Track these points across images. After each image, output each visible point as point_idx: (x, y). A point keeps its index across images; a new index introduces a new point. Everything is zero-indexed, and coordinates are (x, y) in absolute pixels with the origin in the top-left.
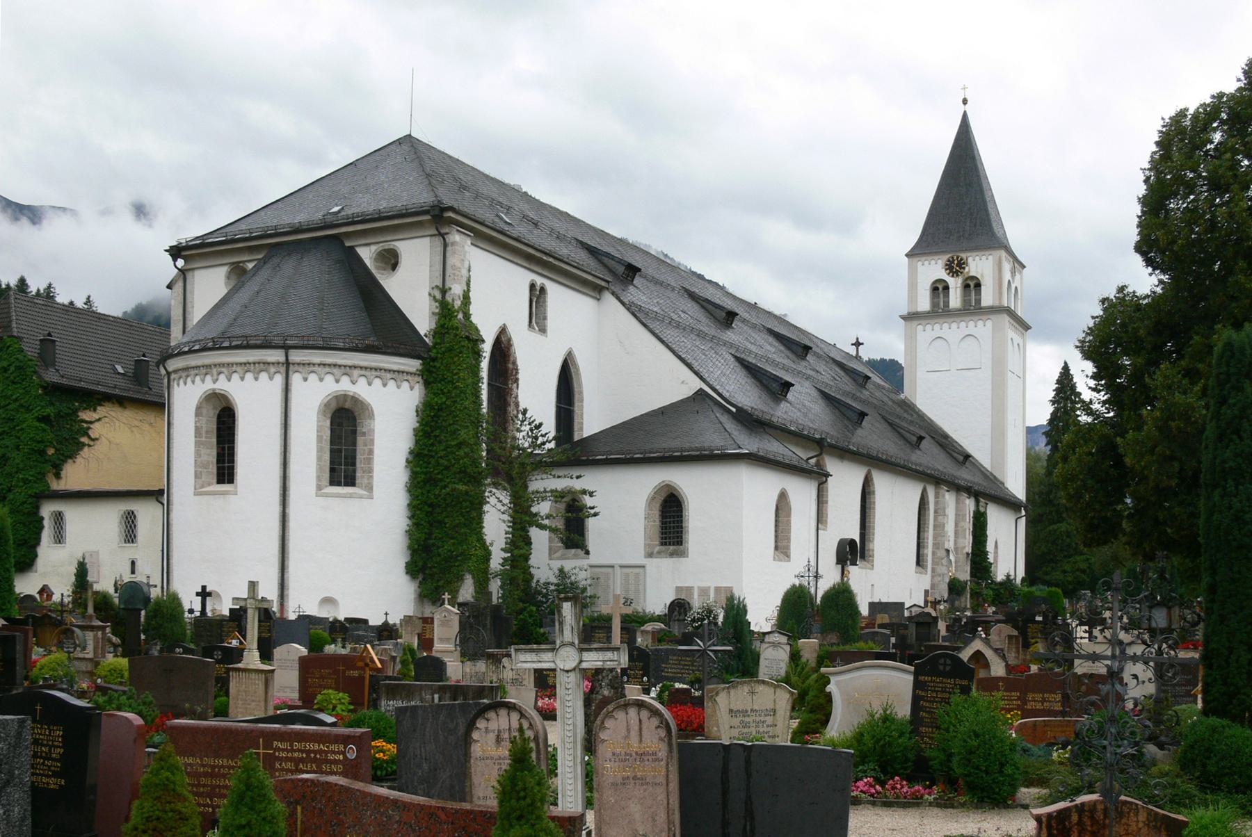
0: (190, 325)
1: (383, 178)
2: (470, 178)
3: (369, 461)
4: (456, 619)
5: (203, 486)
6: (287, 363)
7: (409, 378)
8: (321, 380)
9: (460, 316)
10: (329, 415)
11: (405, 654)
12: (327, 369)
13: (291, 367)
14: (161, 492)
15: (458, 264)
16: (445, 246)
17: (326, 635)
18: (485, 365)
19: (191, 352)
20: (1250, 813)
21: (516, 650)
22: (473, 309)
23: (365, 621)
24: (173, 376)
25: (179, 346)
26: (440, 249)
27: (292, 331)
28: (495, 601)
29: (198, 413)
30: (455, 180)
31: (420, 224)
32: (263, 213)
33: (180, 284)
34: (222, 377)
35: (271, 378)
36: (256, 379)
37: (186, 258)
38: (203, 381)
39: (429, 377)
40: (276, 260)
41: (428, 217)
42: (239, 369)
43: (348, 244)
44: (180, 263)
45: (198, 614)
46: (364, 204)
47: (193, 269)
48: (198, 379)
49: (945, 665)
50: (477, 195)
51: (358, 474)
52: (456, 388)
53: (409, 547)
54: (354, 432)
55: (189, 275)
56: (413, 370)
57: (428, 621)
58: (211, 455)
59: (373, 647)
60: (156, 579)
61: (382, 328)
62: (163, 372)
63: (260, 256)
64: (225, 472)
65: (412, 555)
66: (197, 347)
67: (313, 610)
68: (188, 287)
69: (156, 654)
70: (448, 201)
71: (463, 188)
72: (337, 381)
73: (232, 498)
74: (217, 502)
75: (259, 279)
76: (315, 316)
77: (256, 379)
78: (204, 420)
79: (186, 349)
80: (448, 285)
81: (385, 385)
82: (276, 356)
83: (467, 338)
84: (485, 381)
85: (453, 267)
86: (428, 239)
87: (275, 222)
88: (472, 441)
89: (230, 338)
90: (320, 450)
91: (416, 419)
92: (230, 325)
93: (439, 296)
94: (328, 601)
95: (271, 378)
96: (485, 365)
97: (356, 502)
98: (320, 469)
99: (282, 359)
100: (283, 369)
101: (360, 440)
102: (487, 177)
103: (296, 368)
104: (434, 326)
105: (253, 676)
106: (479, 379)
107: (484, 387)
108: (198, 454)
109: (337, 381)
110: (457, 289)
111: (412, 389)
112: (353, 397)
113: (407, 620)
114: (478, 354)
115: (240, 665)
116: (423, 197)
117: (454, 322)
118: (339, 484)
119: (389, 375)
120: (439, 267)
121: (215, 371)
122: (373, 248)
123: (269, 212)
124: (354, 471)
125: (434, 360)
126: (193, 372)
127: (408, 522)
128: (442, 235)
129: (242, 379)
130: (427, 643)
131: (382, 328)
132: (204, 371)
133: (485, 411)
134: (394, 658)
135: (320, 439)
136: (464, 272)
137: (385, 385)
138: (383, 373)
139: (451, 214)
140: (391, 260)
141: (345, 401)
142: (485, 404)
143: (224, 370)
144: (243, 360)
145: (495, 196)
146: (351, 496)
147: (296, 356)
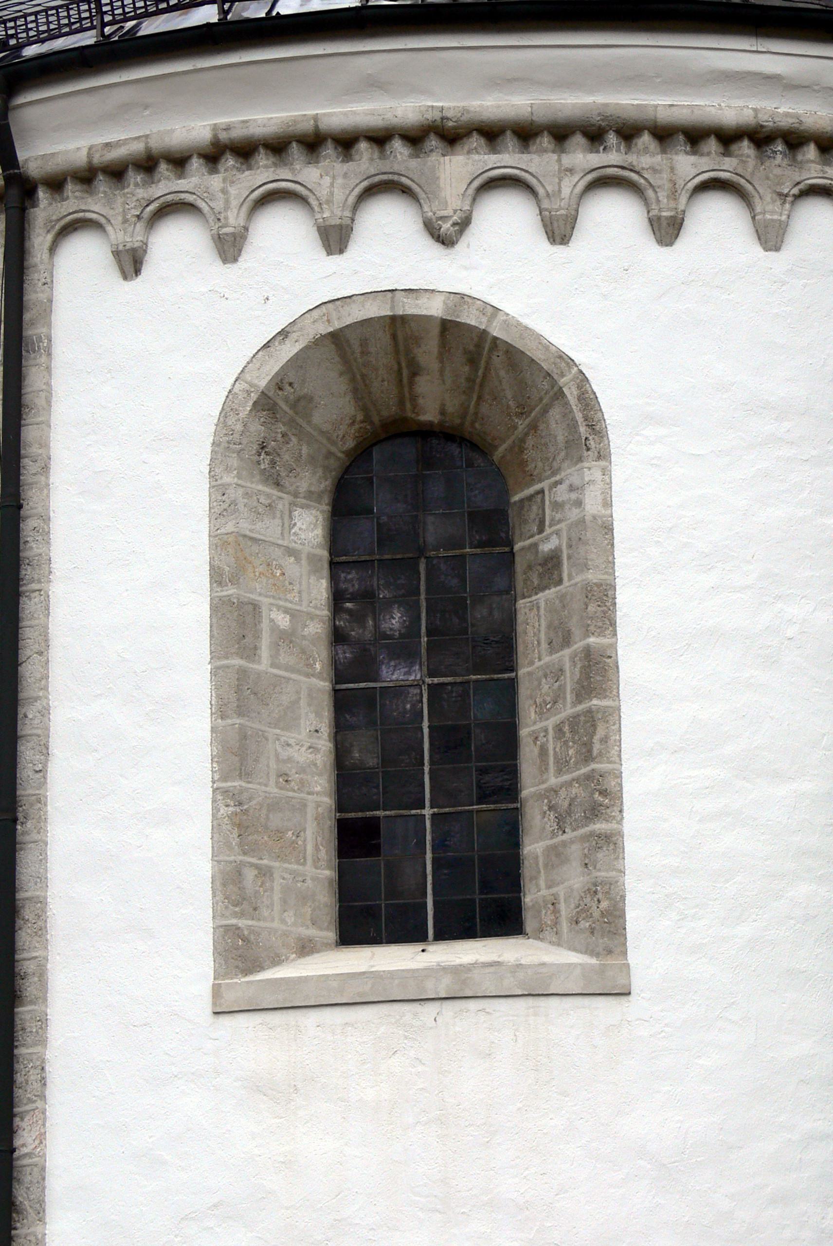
3: (590, 734)
10: (313, 480)
12: (265, 173)
20: (312, 3)
72: (335, 238)
90: (239, 698)
101: (534, 615)
103: (74, 201)
109: (335, 238)
112: (448, 328)
118: (407, 930)
124: (511, 832)
138: (646, 156)
141: (408, 370)
146: (459, 992)
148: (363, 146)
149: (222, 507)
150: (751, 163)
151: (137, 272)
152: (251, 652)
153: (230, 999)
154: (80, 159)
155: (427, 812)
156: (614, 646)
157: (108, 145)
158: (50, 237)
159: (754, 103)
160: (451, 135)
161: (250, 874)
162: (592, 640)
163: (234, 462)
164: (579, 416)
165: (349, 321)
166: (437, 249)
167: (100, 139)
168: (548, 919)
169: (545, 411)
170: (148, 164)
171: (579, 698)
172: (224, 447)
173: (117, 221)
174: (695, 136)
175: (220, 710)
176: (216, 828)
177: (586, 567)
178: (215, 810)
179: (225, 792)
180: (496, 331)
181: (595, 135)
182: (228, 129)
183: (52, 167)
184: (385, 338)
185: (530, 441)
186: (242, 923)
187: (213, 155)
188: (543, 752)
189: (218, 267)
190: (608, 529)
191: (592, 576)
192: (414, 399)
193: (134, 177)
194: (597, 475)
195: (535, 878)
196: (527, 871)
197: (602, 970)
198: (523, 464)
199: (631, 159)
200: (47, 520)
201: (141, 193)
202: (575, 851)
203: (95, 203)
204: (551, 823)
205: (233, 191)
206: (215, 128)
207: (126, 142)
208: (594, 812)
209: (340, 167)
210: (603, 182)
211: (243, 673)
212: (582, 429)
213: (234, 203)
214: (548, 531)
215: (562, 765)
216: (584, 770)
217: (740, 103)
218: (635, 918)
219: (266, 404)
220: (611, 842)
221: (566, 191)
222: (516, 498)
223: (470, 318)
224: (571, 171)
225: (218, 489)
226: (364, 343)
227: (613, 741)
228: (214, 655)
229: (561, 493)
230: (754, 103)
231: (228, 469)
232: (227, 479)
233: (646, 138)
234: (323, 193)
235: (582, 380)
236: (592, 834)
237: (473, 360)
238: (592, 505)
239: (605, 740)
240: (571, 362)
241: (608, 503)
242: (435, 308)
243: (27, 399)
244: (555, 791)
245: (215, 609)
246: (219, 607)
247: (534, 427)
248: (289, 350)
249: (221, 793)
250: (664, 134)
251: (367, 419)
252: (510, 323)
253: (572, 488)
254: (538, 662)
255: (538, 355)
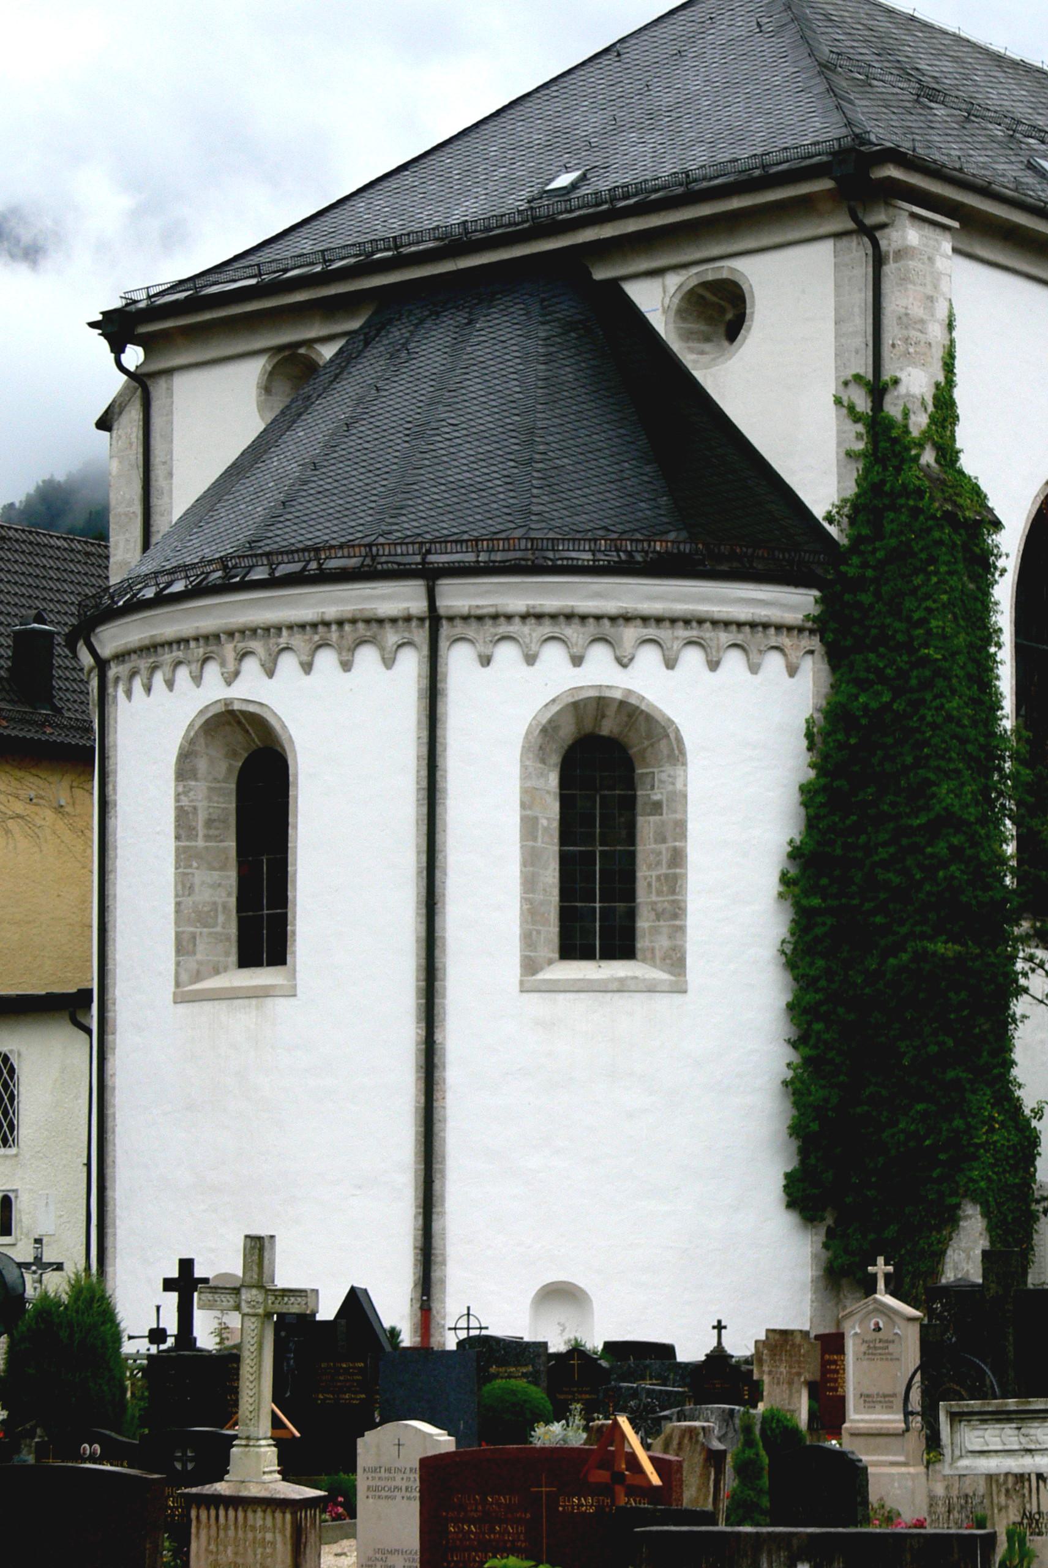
0: (162, 525)
1: (695, 85)
2: (947, 66)
3: (674, 883)
4: (911, 1337)
5: (198, 977)
6: (434, 619)
7: (785, 640)
8: (531, 659)
9: (928, 457)
10: (555, 759)
11: (749, 1443)
12: (547, 629)
13: (445, 630)
14: (85, 995)
15: (917, 311)
16: (879, 260)
17: (537, 1394)
18: (1004, 592)
19: (162, 600)
21: (956, 1417)
22: (965, 436)
23: (668, 1351)
24: (113, 671)
25: (128, 585)
26: (863, 271)
27: (447, 526)
28: (870, 1268)
29: (185, 768)
30: (905, 73)
31: (803, 207)
32: (360, 204)
33: (132, 416)
34: (251, 666)
35: (389, 662)
36: (346, 666)
37: (148, 343)
38: (197, 679)
39: (841, 637)
40: (397, 333)
41: (825, 184)
42: (298, 640)
43: (600, 274)
44: (134, 356)
45: (170, 1342)
46: (644, 159)
47: (169, 372)
48: (183, 675)
49: (184, 1461)
50: (971, 113)
51: (643, 924)
52: (925, 661)
53: (797, 1130)
54: (629, 805)
55: (158, 390)
56: (794, 618)
57: (832, 1344)
58: (220, 887)
59: (648, 1427)
60: (69, 1248)
61: (705, 506)
62: (86, 659)
63: (355, 325)
64: (262, 931)
65: (804, 1153)
66: (178, 587)
67: (510, 1318)
68: (157, 422)
69: (31, 1459)
70: (883, 132)
71: (929, 94)
72: (577, 661)
73: (281, 1005)
74: (239, 1020)
75: (350, 387)
76: (510, 481)
77: (346, 666)
78: (200, 789)
79: (149, 593)
80: (889, 371)
81: (714, 665)
82: (402, 598)
83: (950, 517)
84: (1007, 637)
85: (905, 320)
86: (828, 246)
87: (395, 227)
88: (972, 813)
89: (274, 557)
90: (530, 858)
91: (805, 757)
92: (273, 520)
93: (862, 403)
94: (560, 1295)
95: (389, 662)
96: (1004, 592)
97: (636, 1003)
98: (531, 913)
99: (418, 606)
100: (421, 635)
101: (646, 826)
102: (999, 60)
103: (459, 629)
104: (851, 490)
105: (257, 1518)
106: (988, 636)
107: (1005, 656)
108: (184, 886)
109: (577, 661)
110: (916, 382)
111: (792, 671)
112: (622, 704)
113: (779, 1342)
114: (983, 565)
115: (221, 1488)
116: (804, 125)
117: (911, 476)
118: (585, 953)
119: (724, 637)
120: (862, 323)
121: (229, 650)
122: (673, 281)
123: (378, 199)
124: (631, 915)
125: (858, 584)
126: (168, 657)
127: (788, 1054)
128: (870, 233)
129: (307, 667)
130: (829, 1410)
131: (705, 506)
132: (201, 652)
133: (1008, 724)
134: (715, 1459)
135: (529, 826)
136: (936, 332)
137: (714, 665)
139: (893, 172)
140: (723, 311)
142: (1008, 704)
143: (255, 645)
144: (307, 613)
145: (1021, 110)
146: (621, 987)
147: (457, 596)
148: (591, 620)
149: (525, 776)
150: (749, 636)
151: (488, 663)
152: (535, 839)
153: (527, 986)
154: (465, 611)
155: (598, 905)
156: (685, 847)
157: (477, 607)
158: (448, 643)
159: (752, 611)
160: (627, 618)
161: (534, 933)
162: (677, 844)
163: (531, 755)
164: (675, 747)
165: (581, 697)
166: (620, 668)
167: (474, 603)
168: (649, 955)
169: (659, 740)
170: (495, 617)
171: (669, 867)
172: (526, 750)
173: (481, 641)
174: (727, 624)
175: (524, 864)
176: (522, 914)
177: (675, 812)
178: (522, 906)
179: (526, 899)
180: (643, 707)
181: (687, 622)
182: (534, 607)
183: (451, 612)
184: (594, 705)
185: (649, 749)
186: (532, 954)
187: (524, 617)
188: (650, 885)
189: (524, 666)
190: (685, 796)
191: (678, 816)
192: (600, 726)
193: (489, 622)
194: (682, 773)
195: (644, 937)
196: (639, 933)
197: (676, 982)
198: (644, 758)
199: (702, 634)
200: (446, 771)
201: (492, 630)
202: (665, 930)
203: (471, 631)
204: (653, 916)
205: (534, 635)
206: (528, 606)
207: (487, 606)
208: (675, 916)
209: (582, 630)
210: (690, 643)
211: (533, 847)
212: (676, 752)
213: (534, 640)
214: (656, 791)
215: (659, 893)
216: (671, 898)
217: (746, 610)
218: (689, 961)
219: (544, 730)
220: (682, 929)
221: (675, 647)
222: (639, 771)
223: (633, 701)
224: (677, 638)
225: (524, 767)
226: (585, 705)
227: (684, 887)
228: (522, 839)
229: (664, 776)
230: (752, 611)
231: (529, 759)
232: (528, 763)
233: (708, 625)
234: (574, 640)
235: (677, 730)
236: (674, 926)
237: (630, 716)
238: (679, 786)
239: (681, 886)
240: (673, 723)
241: (685, 785)
242: (618, 695)
243: (438, 716)
244: (655, 903)
245: (522, 819)
246: (523, 819)
247: (652, 745)
248: (555, 708)
249: (524, 900)
250: (715, 623)
251: (579, 733)
252: (649, 704)
253: (669, 776)
254: (647, 846)
255: (660, 719)
